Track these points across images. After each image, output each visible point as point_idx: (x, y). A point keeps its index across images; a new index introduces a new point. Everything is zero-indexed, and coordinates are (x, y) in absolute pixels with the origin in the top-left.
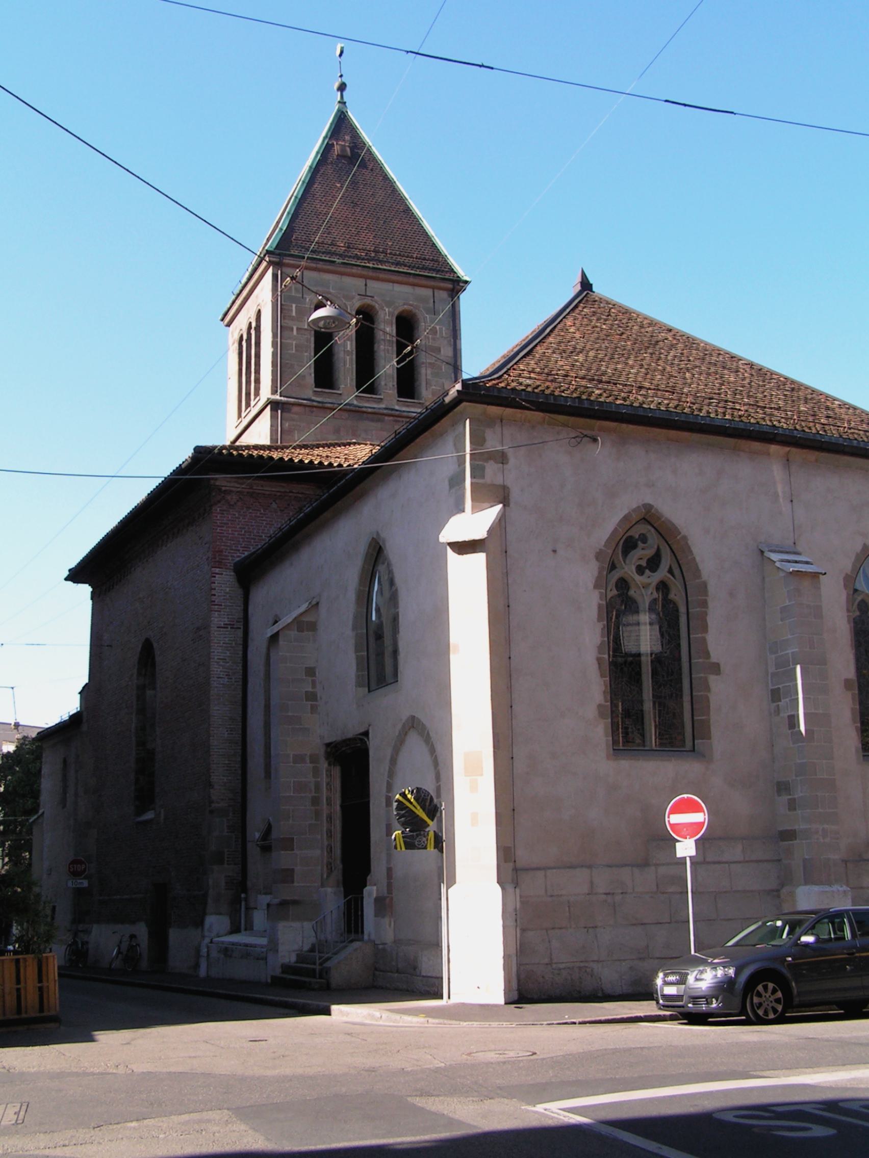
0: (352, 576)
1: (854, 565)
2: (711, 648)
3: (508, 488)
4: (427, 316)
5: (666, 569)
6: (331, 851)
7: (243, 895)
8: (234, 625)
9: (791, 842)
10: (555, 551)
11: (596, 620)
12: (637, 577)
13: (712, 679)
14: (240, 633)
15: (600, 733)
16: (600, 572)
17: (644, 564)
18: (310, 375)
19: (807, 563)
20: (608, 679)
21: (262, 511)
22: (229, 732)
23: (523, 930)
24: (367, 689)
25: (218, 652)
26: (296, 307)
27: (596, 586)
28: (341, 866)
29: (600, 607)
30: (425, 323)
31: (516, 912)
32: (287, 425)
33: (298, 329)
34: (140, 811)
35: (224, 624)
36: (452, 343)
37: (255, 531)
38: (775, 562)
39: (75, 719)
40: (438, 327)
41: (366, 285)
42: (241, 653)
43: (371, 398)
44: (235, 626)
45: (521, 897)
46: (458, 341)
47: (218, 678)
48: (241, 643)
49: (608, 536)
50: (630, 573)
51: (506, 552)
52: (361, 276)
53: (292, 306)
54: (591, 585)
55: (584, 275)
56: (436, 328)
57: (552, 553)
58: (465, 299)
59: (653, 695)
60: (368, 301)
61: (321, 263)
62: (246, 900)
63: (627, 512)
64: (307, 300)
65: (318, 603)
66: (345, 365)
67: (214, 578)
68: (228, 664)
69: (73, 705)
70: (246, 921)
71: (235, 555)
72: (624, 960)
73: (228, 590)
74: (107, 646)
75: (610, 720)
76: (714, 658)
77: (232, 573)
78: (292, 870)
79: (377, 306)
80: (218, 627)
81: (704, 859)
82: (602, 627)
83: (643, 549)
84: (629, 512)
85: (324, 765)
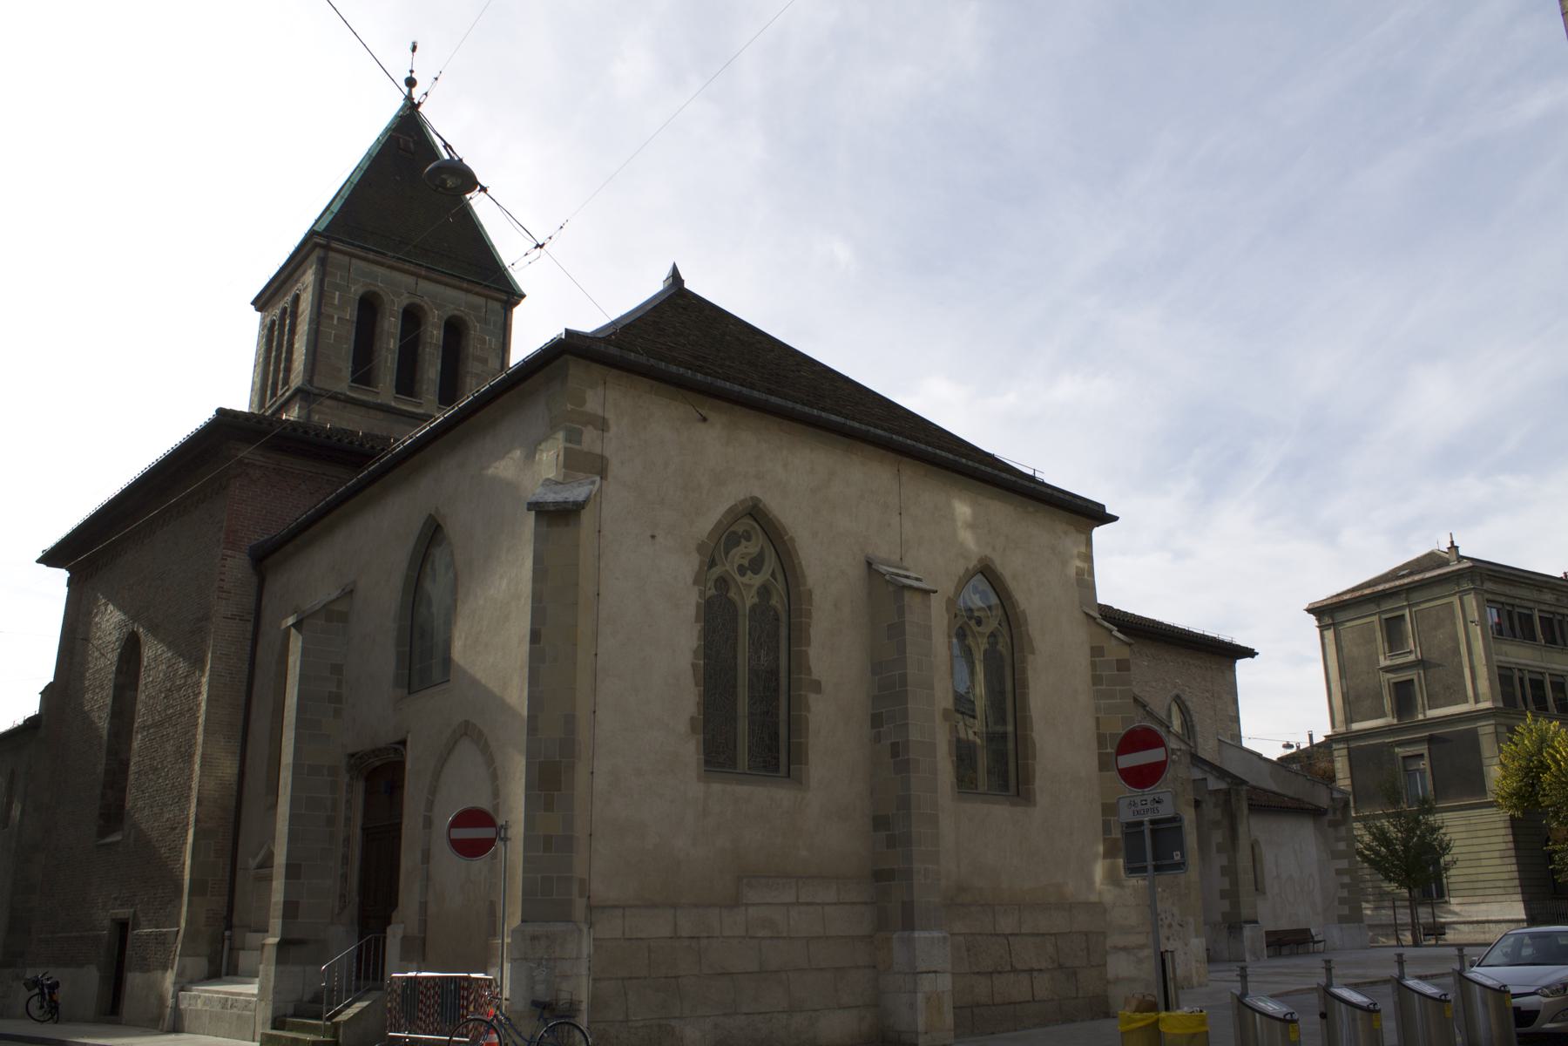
0: (399, 558)
1: (956, 588)
2: (813, 663)
3: (607, 459)
4: (478, 325)
5: (770, 572)
7: (227, 933)
9: (887, 883)
10: (653, 537)
11: (693, 620)
12: (737, 577)
13: (812, 697)
14: (250, 627)
15: (691, 751)
17: (747, 564)
19: (917, 579)
23: (594, 980)
24: (406, 691)
26: (340, 295)
27: (696, 582)
28: (357, 899)
32: (317, 417)
33: (338, 318)
34: (103, 833)
36: (501, 356)
39: (31, 724)
42: (249, 649)
45: (594, 939)
46: (506, 355)
48: (250, 637)
49: (712, 527)
51: (599, 531)
52: (412, 274)
53: (335, 294)
54: (690, 580)
55: (675, 270)
57: (650, 539)
58: (518, 313)
60: (417, 300)
62: (230, 938)
63: (733, 503)
64: (353, 289)
65: (352, 591)
66: (386, 362)
67: (223, 569)
68: (232, 661)
69: (32, 707)
70: (228, 964)
72: (709, 1016)
76: (815, 676)
77: (248, 558)
78: (298, 903)
81: (798, 898)
84: (736, 505)
85: (344, 778)
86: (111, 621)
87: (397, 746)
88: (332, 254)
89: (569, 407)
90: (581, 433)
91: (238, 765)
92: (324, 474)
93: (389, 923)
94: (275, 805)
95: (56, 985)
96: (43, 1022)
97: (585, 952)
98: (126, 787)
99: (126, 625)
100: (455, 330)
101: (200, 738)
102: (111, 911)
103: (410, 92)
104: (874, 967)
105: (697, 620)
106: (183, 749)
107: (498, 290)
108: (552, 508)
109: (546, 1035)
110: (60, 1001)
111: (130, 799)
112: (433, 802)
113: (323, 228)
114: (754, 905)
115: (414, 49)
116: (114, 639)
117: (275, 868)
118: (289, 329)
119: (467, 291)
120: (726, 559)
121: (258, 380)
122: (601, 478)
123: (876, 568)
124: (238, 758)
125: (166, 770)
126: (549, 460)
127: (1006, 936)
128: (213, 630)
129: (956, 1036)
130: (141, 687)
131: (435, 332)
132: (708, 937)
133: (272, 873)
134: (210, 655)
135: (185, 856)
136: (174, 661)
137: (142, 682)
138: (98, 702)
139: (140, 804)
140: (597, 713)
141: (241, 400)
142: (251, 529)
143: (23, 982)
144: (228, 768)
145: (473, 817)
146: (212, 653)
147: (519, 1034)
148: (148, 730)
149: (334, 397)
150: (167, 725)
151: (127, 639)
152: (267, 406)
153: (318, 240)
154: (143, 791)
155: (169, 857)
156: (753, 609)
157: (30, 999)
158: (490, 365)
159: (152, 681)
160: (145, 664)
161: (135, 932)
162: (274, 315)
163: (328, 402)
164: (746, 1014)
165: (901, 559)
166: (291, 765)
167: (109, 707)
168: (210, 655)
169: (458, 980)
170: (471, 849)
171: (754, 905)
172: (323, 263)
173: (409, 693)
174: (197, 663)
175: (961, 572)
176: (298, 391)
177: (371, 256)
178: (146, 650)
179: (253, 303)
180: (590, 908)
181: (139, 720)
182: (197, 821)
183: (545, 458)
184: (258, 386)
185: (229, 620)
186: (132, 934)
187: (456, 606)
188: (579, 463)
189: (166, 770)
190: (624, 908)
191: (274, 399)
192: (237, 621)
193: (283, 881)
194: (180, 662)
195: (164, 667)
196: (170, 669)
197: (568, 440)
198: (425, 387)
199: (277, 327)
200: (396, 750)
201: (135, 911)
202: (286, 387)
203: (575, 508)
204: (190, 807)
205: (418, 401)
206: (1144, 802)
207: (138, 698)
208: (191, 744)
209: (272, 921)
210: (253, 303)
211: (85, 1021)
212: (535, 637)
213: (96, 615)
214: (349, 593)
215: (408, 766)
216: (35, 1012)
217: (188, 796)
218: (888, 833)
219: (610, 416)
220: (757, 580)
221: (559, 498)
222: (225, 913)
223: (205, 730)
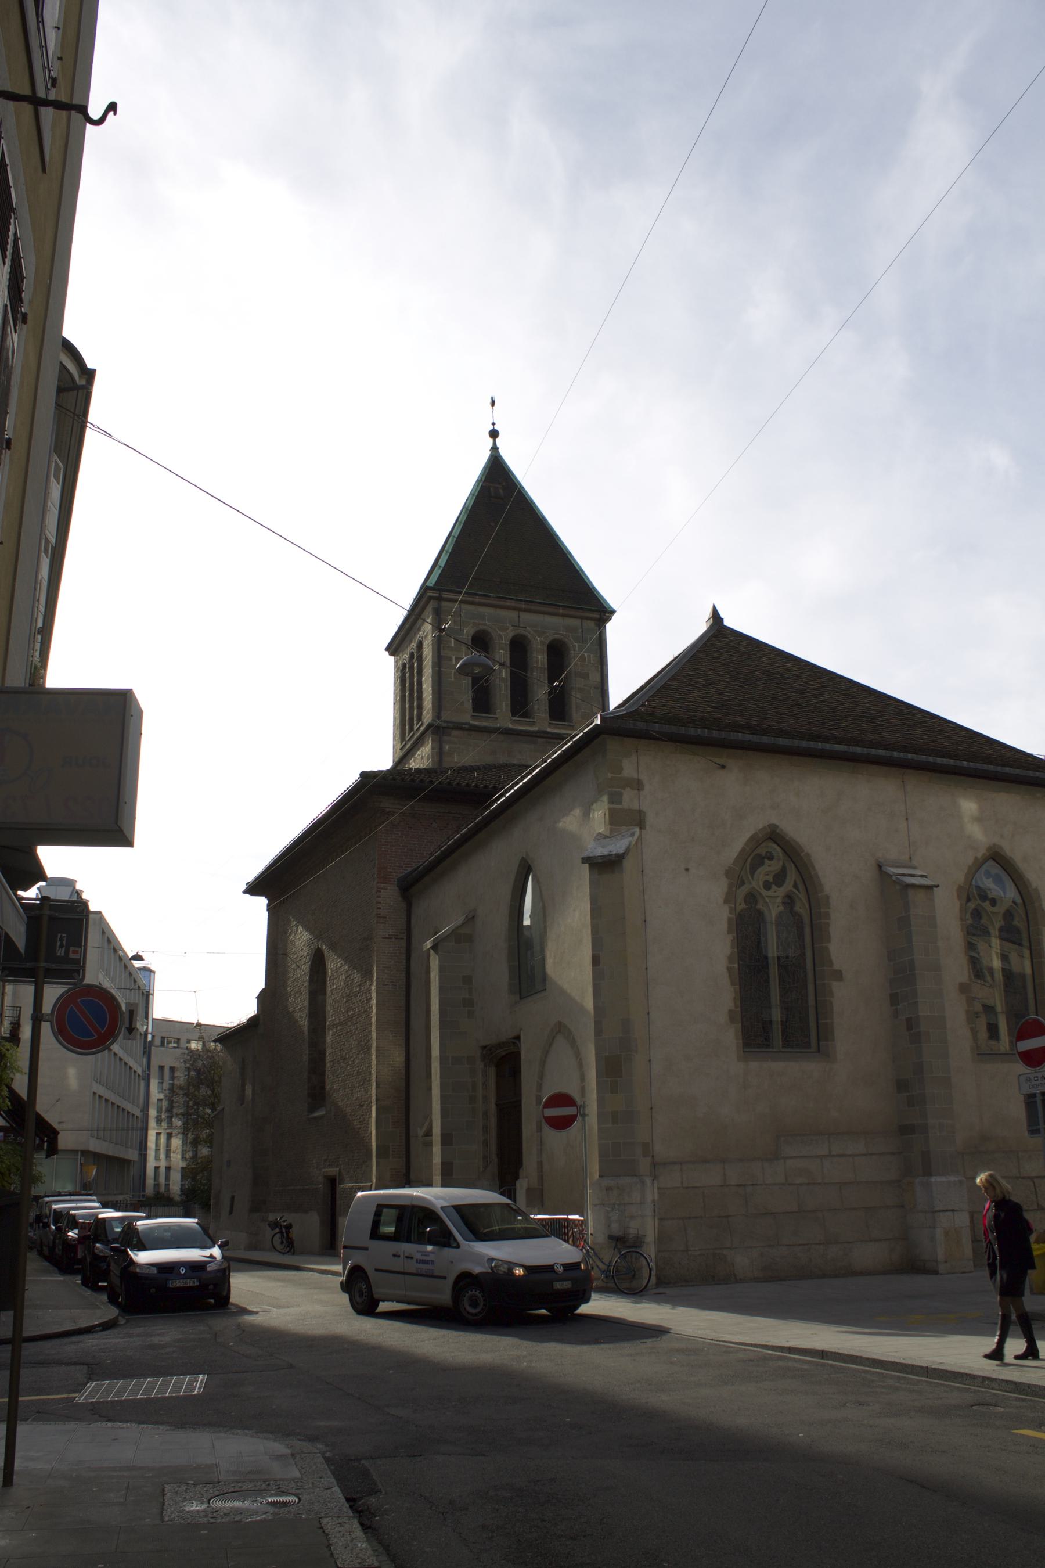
3: (644, 813)
4: (577, 644)
6: (487, 1146)
8: (397, 935)
10: (687, 870)
12: (764, 892)
14: (404, 943)
15: (731, 1037)
16: (730, 886)
18: (469, 701)
19: (922, 876)
20: (738, 986)
21: (423, 830)
22: (394, 1035)
23: (661, 1219)
24: (518, 996)
25: (383, 961)
28: (496, 1160)
29: (729, 920)
30: (574, 651)
31: (654, 1202)
32: (447, 747)
34: (312, 1109)
35: (389, 935)
37: (417, 849)
38: (892, 876)
40: (586, 655)
41: (519, 617)
43: (525, 721)
44: (399, 937)
47: (384, 985)
49: (736, 855)
50: (758, 889)
51: (642, 871)
55: (715, 611)
56: (584, 655)
59: (780, 1000)
60: (521, 631)
61: (477, 597)
63: (754, 832)
64: (465, 631)
65: (473, 917)
67: (379, 899)
71: (399, 871)
73: (392, 903)
74: (282, 954)
75: (740, 1025)
77: (397, 888)
79: (529, 636)
80: (383, 938)
82: (732, 938)
83: (769, 866)
86: (302, 939)
87: (514, 1041)
88: (444, 604)
89: (610, 775)
90: (621, 795)
91: (404, 1055)
92: (449, 813)
93: (517, 1178)
94: (430, 1089)
95: (289, 1227)
96: (284, 1254)
97: (649, 1198)
98: (325, 1071)
99: (313, 943)
100: (557, 652)
101: (374, 1034)
102: (323, 1170)
103: (495, 443)
104: (903, 1206)
105: (729, 932)
106: (362, 1043)
107: (590, 610)
108: (600, 861)
109: (619, 1261)
110: (294, 1238)
111: (328, 1081)
112: (541, 1084)
113: (434, 583)
114: (791, 1158)
115: (493, 403)
116: (305, 954)
117: (433, 1136)
118: (417, 672)
119: (563, 616)
120: (752, 878)
121: (398, 716)
122: (641, 828)
123: (884, 870)
124: (404, 1049)
125: (352, 1059)
126: (599, 815)
127: (1031, 1178)
128: (376, 949)
129: (975, 1266)
130: (329, 993)
131: (540, 657)
132: (753, 1185)
133: (432, 1140)
134: (375, 968)
135: (371, 1126)
136: (350, 972)
137: (329, 989)
138: (299, 1004)
139: (336, 1086)
140: (650, 1014)
141: (383, 760)
142: (397, 865)
143: (267, 1223)
144: (398, 1057)
145: (562, 1099)
146: (376, 967)
147: (601, 1260)
148: (336, 1027)
149: (459, 727)
150: (349, 1023)
151: (315, 954)
152: (407, 739)
153: (431, 594)
154: (337, 1076)
155: (360, 1128)
156: (780, 915)
157: (273, 1236)
158: (590, 678)
159: (336, 988)
160: (330, 974)
161: (342, 1186)
162: (404, 659)
163: (455, 733)
164: (787, 1245)
165: (910, 858)
166: (439, 1057)
167: (307, 1009)
168: (375, 968)
169: (561, 1221)
170: (562, 1123)
171: (791, 1158)
172: (438, 613)
173: (521, 998)
174: (367, 974)
175: (970, 861)
176: (429, 726)
177: (477, 599)
178: (330, 964)
179: (387, 649)
180: (654, 1165)
181: (330, 1020)
182: (377, 1100)
183: (596, 816)
184: (398, 721)
185: (387, 940)
186: (340, 1187)
187: (546, 932)
188: (619, 819)
189: (352, 1059)
190: (681, 1164)
191: (412, 733)
192: (393, 940)
193: (440, 1147)
194: (354, 973)
195: (344, 978)
196: (348, 979)
197: (611, 802)
198: (536, 707)
199: (407, 669)
200: (514, 1043)
201: (340, 1170)
202: (420, 723)
203: (617, 859)
204: (372, 1088)
205: (532, 720)
206: (1036, 1079)
207: (327, 1002)
208: (369, 1039)
209: (434, 1177)
210: (387, 649)
211: (311, 1253)
212: (596, 961)
213: (290, 935)
214: (471, 919)
215: (523, 1056)
216: (279, 1247)
217: (370, 1080)
218: (908, 1094)
219: (644, 777)
220: (781, 891)
221: (605, 852)
222: (404, 1171)
223: (377, 1028)
